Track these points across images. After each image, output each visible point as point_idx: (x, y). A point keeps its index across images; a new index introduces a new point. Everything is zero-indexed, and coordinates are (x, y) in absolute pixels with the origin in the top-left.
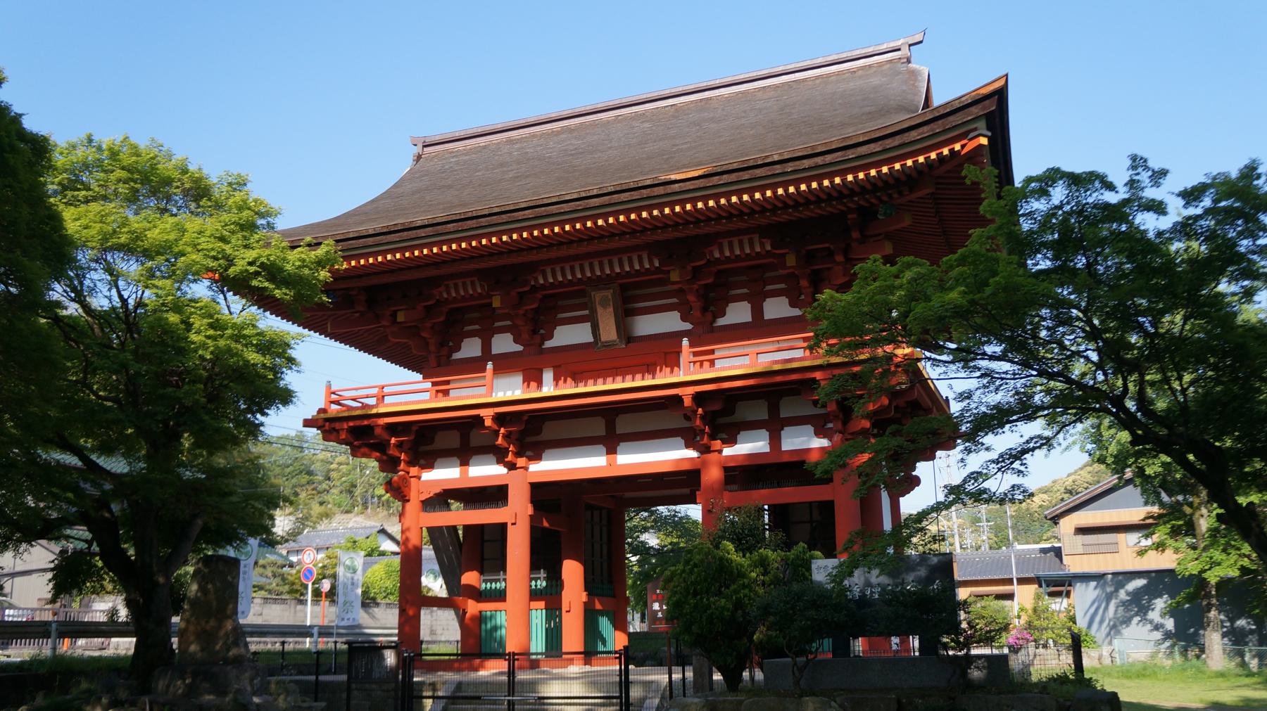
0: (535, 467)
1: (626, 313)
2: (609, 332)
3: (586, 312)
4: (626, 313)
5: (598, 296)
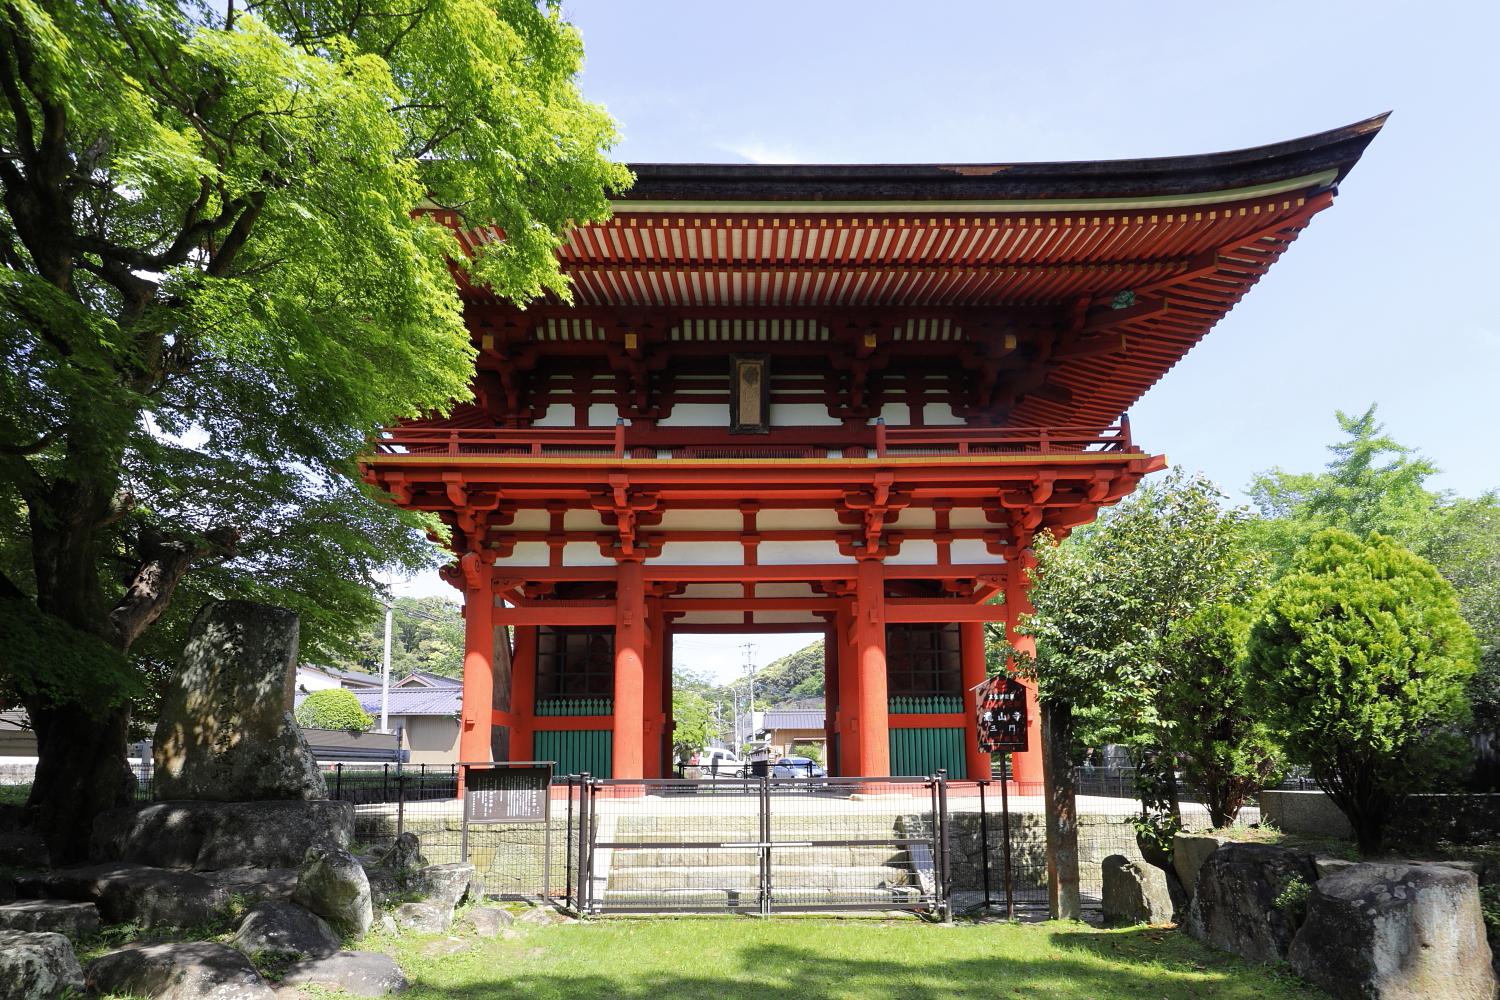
0: (890, 560)
1: (768, 401)
2: (750, 415)
3: (728, 392)
4: (768, 401)
5: (743, 367)
